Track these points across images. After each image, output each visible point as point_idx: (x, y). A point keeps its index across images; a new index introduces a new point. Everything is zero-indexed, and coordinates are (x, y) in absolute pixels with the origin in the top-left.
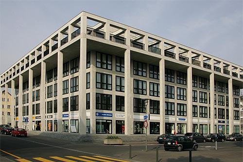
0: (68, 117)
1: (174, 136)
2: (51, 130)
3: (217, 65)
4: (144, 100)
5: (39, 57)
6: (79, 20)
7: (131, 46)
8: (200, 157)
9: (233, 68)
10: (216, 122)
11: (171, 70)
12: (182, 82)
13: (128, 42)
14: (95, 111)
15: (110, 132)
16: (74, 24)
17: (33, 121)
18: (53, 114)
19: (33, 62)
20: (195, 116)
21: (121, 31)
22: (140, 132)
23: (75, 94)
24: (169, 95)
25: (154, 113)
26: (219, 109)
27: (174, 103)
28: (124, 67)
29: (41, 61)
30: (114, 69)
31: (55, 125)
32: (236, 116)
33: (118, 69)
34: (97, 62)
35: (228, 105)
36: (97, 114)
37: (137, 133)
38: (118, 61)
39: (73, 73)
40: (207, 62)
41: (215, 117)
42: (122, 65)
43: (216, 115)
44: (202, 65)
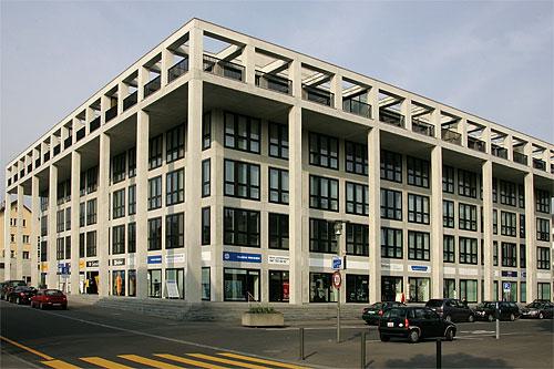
2: (123, 294)
3: (499, 143)
4: (332, 224)
5: (95, 125)
6: (186, 38)
7: (303, 97)
8: (460, 355)
9: (536, 149)
10: (497, 273)
12: (418, 180)
13: (297, 90)
14: (222, 248)
15: (256, 298)
16: (174, 49)
17: (81, 273)
18: (127, 255)
19: (81, 134)
21: (281, 63)
23: (177, 209)
24: (391, 212)
26: (503, 243)
28: (287, 147)
29: (99, 132)
32: (541, 261)
33: (275, 151)
34: (225, 134)
35: (523, 236)
37: (316, 299)
38: (275, 133)
39: (173, 161)
42: (284, 143)
43: (496, 257)
44: (464, 142)
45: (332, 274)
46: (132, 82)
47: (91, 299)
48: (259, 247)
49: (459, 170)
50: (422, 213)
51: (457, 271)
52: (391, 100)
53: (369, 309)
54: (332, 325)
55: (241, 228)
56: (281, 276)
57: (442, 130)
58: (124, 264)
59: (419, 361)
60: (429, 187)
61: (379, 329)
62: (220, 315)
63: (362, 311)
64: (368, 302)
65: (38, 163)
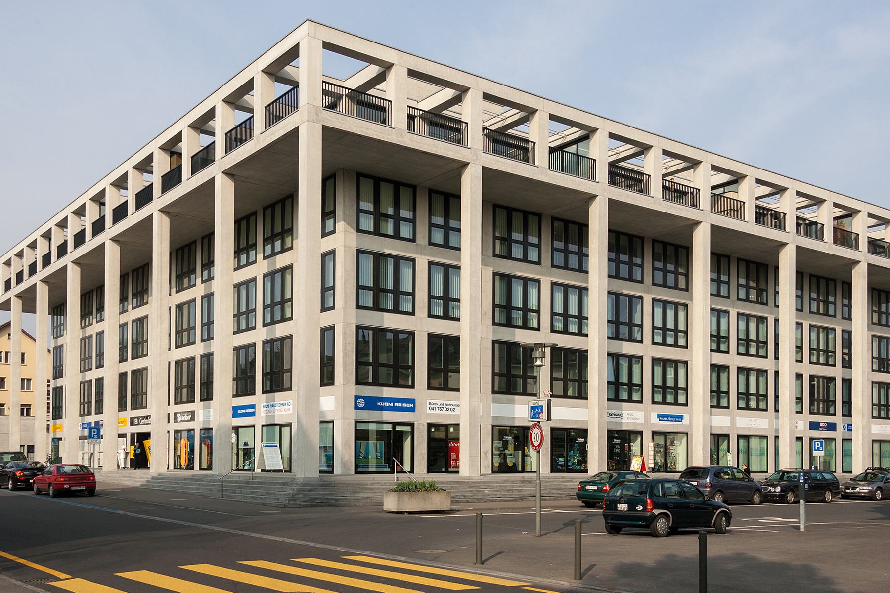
0: (253, 414)
1: (641, 478)
2: (190, 467)
3: (809, 215)
4: (529, 350)
5: (144, 197)
6: (293, 54)
7: (485, 151)
8: (738, 558)
9: (873, 222)
10: (802, 425)
11: (631, 237)
12: (670, 278)
13: (475, 137)
14: (353, 390)
15: (407, 467)
16: (275, 72)
17: (120, 436)
18: (197, 406)
19: (120, 213)
20: (719, 406)
21: (448, 94)
22: (515, 465)
23: (281, 330)
24: (624, 330)
25: (565, 396)
26: (812, 377)
27: (641, 358)
28: (459, 230)
29: (152, 209)
30: (422, 237)
31: (204, 448)
32: (879, 405)
33: (438, 237)
34: (359, 211)
35: (847, 364)
36: (361, 403)
37: (504, 468)
38: (439, 207)
39: (274, 254)
40: (772, 204)
41: (794, 408)
42: (453, 224)
43: (799, 400)
44: (750, 213)
45: (528, 428)
46: (206, 128)
47: (138, 478)
48: (413, 387)
49: (739, 260)
50: (676, 331)
51: (733, 421)
52: (627, 150)
53: (588, 483)
54: (529, 508)
55: (383, 358)
56: (447, 431)
57: (713, 196)
58: (192, 419)
59: (668, 565)
60: (687, 289)
61: (606, 516)
62: (348, 496)
63: (577, 485)
64: (586, 471)
65: (47, 260)
